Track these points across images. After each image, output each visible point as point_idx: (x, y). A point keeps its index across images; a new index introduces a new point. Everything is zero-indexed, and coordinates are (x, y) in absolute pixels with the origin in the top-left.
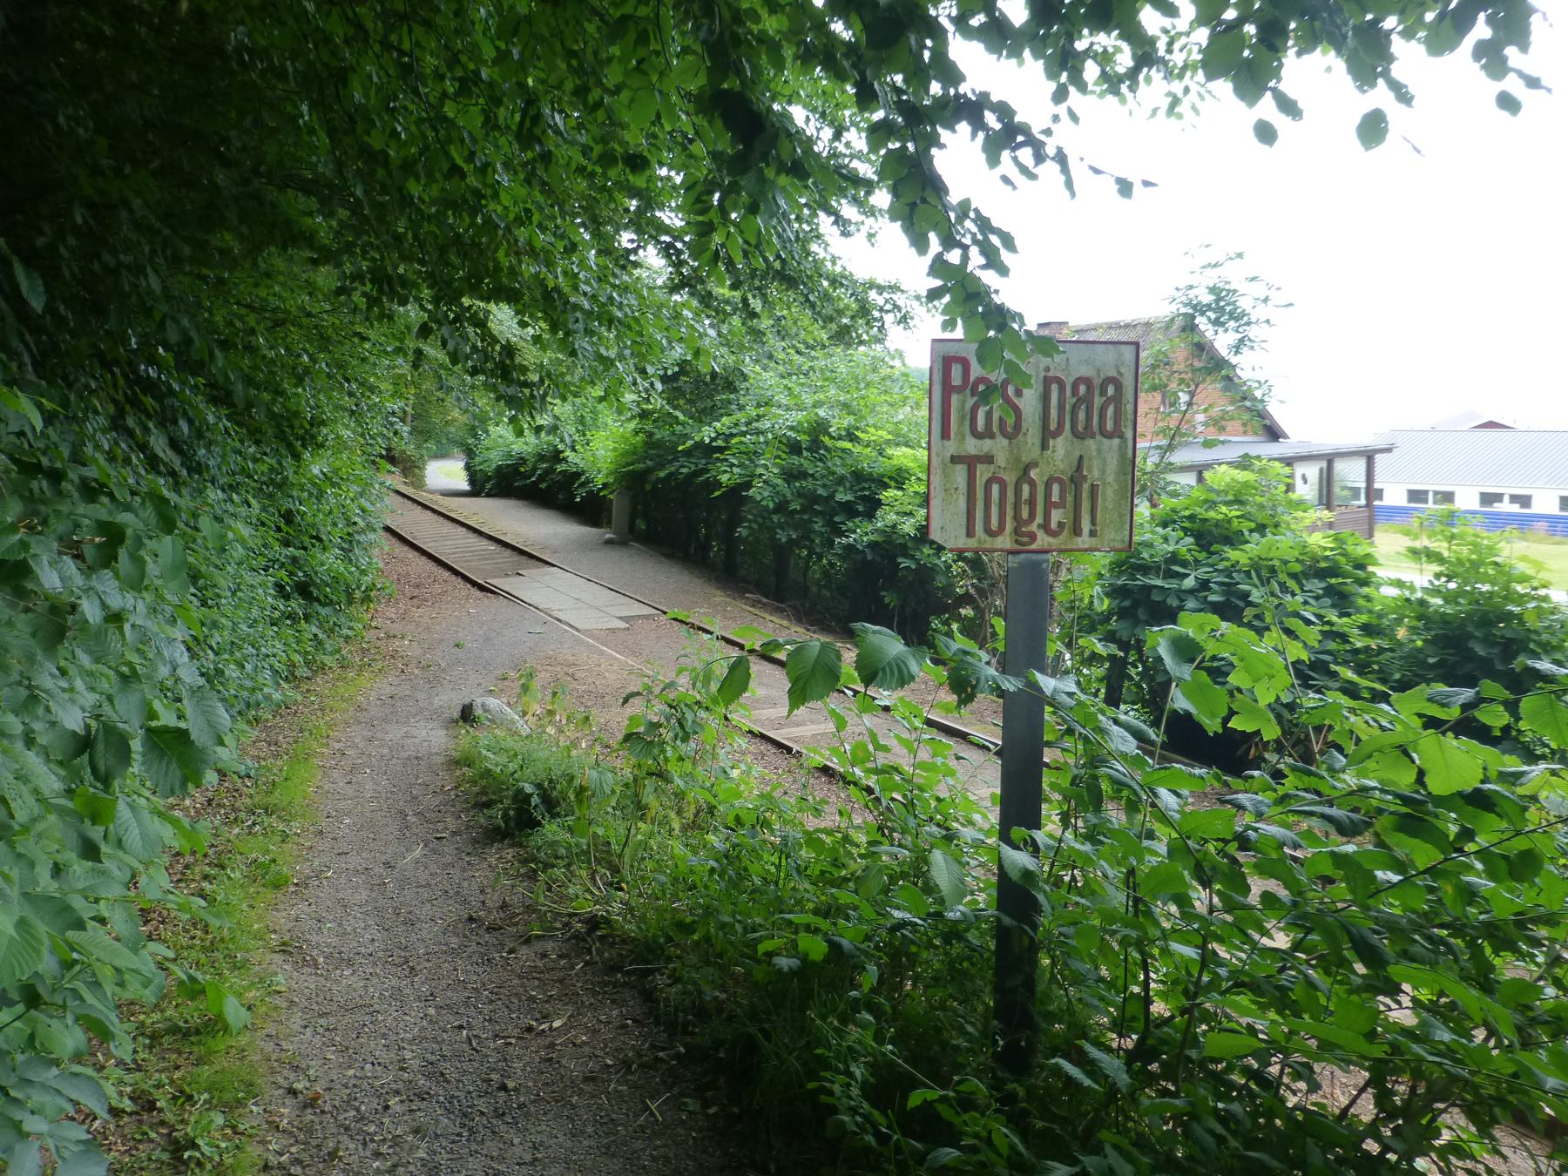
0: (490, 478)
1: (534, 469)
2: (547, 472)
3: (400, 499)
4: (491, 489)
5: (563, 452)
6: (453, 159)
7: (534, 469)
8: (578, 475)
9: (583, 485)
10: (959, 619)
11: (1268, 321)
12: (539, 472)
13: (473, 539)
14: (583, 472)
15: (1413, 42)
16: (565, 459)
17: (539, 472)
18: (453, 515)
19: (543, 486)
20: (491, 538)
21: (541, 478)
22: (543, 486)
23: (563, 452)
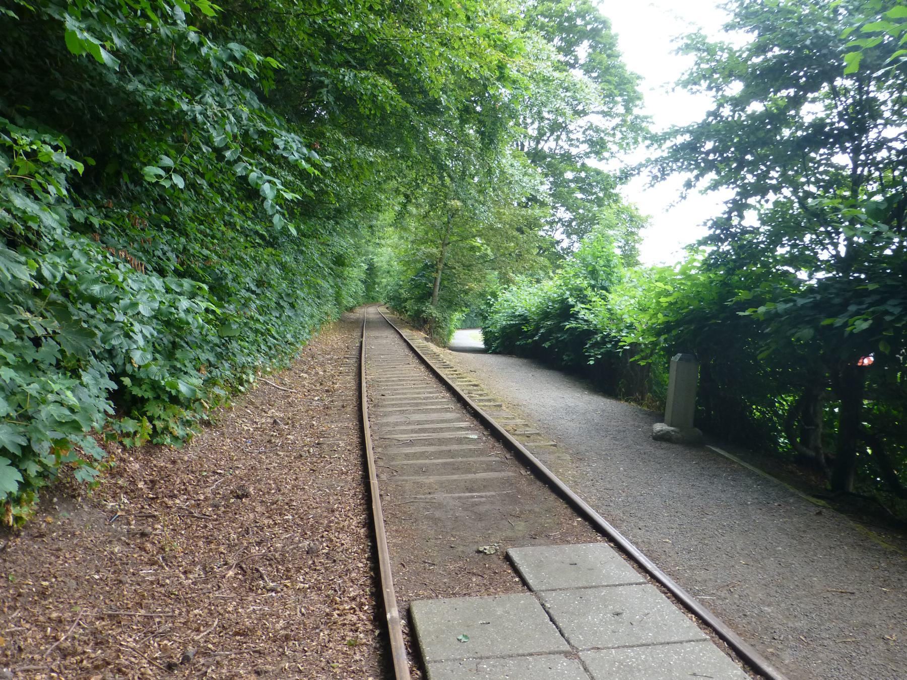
0: (497, 338)
1: (537, 328)
2: (550, 332)
3: (407, 351)
4: (497, 348)
5: (573, 306)
6: (74, 396)
7: (537, 328)
8: (589, 334)
9: (596, 345)
10: (55, 504)
11: (667, 210)
12: (542, 331)
13: (453, 413)
14: (596, 331)
15: (686, 90)
16: (575, 316)
17: (542, 331)
18: (443, 373)
19: (547, 345)
20: (476, 415)
21: (544, 338)
22: (547, 345)
23: (573, 306)
